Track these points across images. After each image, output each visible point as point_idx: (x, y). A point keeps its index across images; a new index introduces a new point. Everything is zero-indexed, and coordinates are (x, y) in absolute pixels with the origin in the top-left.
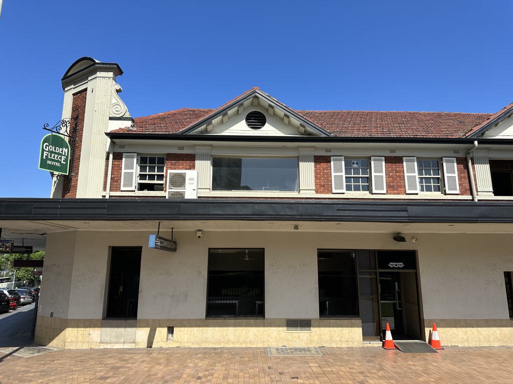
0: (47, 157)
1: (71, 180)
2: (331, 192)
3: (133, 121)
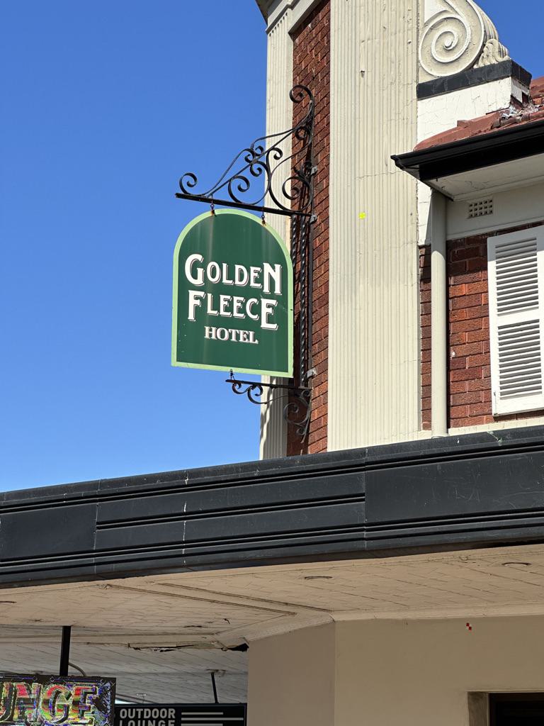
0: (200, 311)
1: (308, 399)
3: (519, 74)
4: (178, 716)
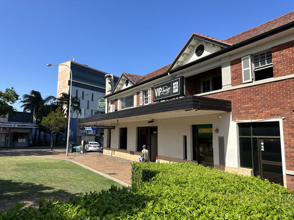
2: (241, 83)
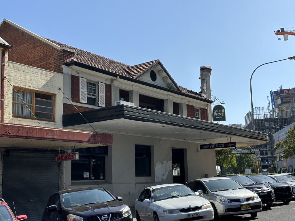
4: (224, 145)
